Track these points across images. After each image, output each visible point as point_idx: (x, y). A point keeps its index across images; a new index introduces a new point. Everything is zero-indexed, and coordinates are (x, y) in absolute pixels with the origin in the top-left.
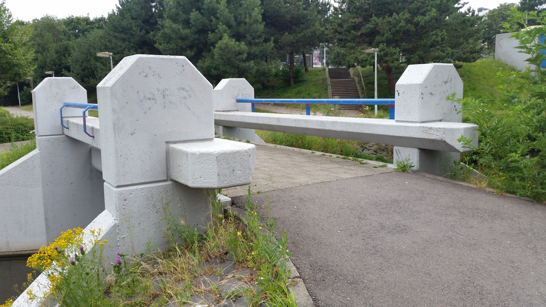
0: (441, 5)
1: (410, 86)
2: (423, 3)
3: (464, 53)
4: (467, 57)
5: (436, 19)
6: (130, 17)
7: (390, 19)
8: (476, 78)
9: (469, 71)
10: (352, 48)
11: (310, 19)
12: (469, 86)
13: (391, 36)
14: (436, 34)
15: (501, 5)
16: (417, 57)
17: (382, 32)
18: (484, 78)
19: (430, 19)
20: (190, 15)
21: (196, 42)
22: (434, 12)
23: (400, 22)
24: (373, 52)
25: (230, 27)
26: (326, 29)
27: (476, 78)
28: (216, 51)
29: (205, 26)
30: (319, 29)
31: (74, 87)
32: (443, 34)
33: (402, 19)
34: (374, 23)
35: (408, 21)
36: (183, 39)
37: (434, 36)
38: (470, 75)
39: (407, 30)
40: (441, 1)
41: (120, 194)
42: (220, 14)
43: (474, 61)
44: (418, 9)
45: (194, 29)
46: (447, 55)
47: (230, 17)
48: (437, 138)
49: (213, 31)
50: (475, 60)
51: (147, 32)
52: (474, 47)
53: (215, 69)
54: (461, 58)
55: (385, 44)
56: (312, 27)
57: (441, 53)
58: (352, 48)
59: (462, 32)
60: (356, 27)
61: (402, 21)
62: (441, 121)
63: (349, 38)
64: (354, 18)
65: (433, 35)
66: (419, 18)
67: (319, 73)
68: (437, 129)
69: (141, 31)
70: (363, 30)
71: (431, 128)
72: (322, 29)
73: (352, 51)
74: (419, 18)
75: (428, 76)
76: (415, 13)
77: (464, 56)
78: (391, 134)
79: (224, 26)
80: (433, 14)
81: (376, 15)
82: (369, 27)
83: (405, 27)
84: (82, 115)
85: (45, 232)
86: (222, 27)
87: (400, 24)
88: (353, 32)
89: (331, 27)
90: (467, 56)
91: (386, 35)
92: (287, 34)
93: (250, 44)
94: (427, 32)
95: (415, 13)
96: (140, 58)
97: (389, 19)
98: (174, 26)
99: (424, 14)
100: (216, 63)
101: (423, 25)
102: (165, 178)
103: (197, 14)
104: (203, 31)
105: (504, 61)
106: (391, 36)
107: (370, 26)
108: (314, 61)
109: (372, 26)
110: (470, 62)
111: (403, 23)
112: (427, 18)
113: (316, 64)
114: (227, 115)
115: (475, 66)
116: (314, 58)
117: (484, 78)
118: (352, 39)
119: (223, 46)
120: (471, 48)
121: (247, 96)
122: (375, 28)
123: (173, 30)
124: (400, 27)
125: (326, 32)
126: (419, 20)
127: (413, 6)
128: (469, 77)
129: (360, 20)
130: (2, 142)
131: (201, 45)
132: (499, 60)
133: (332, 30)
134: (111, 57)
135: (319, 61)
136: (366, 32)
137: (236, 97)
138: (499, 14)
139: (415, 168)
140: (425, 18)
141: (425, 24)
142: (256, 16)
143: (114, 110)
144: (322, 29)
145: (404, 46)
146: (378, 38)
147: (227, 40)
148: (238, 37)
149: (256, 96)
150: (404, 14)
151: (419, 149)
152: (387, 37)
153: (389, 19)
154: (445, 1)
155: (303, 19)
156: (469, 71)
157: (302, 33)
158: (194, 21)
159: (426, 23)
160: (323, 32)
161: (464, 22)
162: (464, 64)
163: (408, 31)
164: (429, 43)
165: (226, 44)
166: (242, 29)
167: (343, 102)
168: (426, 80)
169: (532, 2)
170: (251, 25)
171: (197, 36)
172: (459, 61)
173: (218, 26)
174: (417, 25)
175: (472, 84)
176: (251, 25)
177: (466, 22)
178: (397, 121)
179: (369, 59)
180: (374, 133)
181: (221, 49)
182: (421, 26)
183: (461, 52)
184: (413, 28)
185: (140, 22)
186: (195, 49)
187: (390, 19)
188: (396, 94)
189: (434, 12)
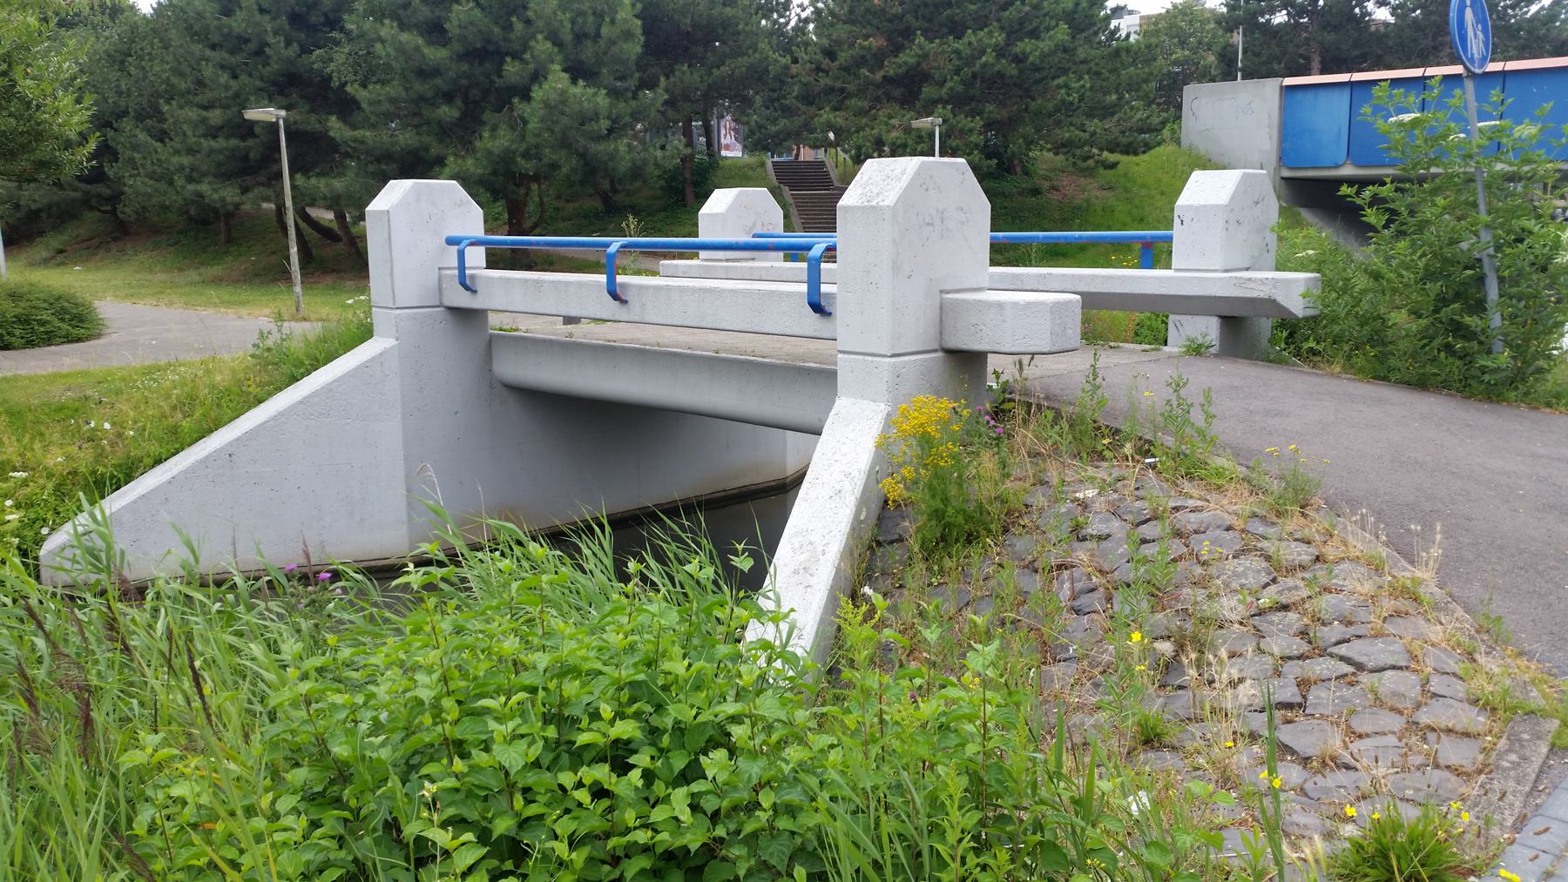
0: (1074, 12)
1: (870, 211)
2: (1036, 7)
3: (1123, 132)
4: (1131, 143)
5: (1065, 50)
6: (256, 7)
7: (957, 45)
8: (1144, 192)
9: (1126, 175)
10: (861, 113)
11: (744, 30)
12: (1129, 212)
13: (960, 88)
14: (1066, 86)
15: (1175, 7)
16: (1021, 140)
17: (937, 75)
18: (1162, 193)
19: (1053, 47)
20: (451, 11)
21: (464, 82)
22: (1062, 33)
23: (983, 52)
24: (929, 126)
25: (558, 43)
26: (795, 61)
27: (1144, 192)
28: (532, 112)
29: (489, 41)
30: (776, 61)
31: (461, 204)
32: (1083, 86)
33: (990, 46)
34: (919, 52)
35: (1001, 52)
36: (424, 73)
37: (1063, 91)
38: (1129, 185)
39: (999, 72)
40: (1077, 5)
41: (895, 366)
42: (535, 11)
43: (1144, 152)
44: (1022, 22)
45: (457, 47)
46: (1092, 136)
47: (561, 21)
48: (1262, 295)
49: (516, 56)
50: (1148, 147)
51: (305, 50)
52: (1148, 117)
53: (526, 155)
54: (1118, 145)
55: (949, 107)
56: (750, 52)
57: (1077, 132)
58: (861, 113)
59: (1113, 78)
60: (878, 59)
61: (989, 50)
62: (1247, 269)
63: (851, 87)
64: (866, 37)
65: (1059, 87)
66: (1024, 46)
67: (750, 173)
68: (1261, 280)
69: (288, 44)
70: (891, 68)
71: (1250, 279)
72: (783, 61)
73: (864, 121)
74: (1024, 46)
75: (1235, 191)
76: (1016, 31)
77: (1124, 140)
78: (1171, 292)
79: (549, 45)
80: (1060, 36)
81: (925, 33)
82: (905, 63)
83: (993, 65)
84: (456, 265)
85: (405, 518)
86: (542, 46)
87: (984, 59)
88: (864, 71)
89: (806, 57)
90: (1131, 139)
91: (949, 84)
92: (685, 67)
93: (614, 93)
94: (1043, 79)
95: (1016, 31)
96: (923, 163)
97: (956, 45)
98: (405, 37)
99: (1035, 34)
100: (531, 140)
101: (1038, 62)
102: (937, 347)
103: (472, 9)
104: (486, 53)
105: (1202, 152)
106: (960, 88)
107: (907, 57)
108: (723, 141)
109: (912, 61)
110: (1136, 153)
111: (988, 58)
112: (1045, 45)
113: (727, 147)
114: (751, 268)
115: (1137, 164)
116: (723, 132)
117: (1162, 193)
118: (859, 90)
119: (553, 97)
120: (1141, 120)
121: (770, 227)
122: (919, 64)
123: (401, 50)
124: (984, 65)
125: (794, 69)
126: (1028, 49)
127: (1011, 14)
128: (1126, 190)
129: (882, 42)
130: (7, 347)
131: (475, 93)
132: (1190, 148)
133: (809, 65)
134: (281, 122)
135: (736, 139)
136: (897, 75)
137: (751, 229)
138: (1171, 28)
139: (1212, 350)
140: (1041, 45)
141: (1042, 62)
142: (626, 21)
143: (894, 241)
144: (783, 61)
145: (990, 112)
146: (928, 91)
147: (558, 80)
148: (577, 71)
149: (487, 231)
150: (990, 33)
151: (1220, 317)
152: (951, 89)
153: (956, 45)
154: (1084, 5)
155: (724, 29)
156: (1126, 175)
157: (722, 68)
158: (460, 27)
159: (1044, 56)
160: (787, 68)
161: (1117, 52)
162: (1124, 159)
163: (1000, 75)
164: (1050, 106)
165: (563, 92)
166: (588, 52)
167: (1045, 237)
168: (1233, 198)
169: (1253, 4)
170: (612, 42)
171: (465, 67)
172: (1112, 151)
173: (532, 43)
174: (1019, 60)
175: (1137, 207)
176: (612, 42)
177: (1124, 55)
178: (1177, 270)
179: (910, 142)
180: (1137, 291)
181: (547, 104)
182: (1032, 64)
183: (1116, 131)
184: (1012, 70)
185: (283, 21)
186: (459, 102)
187: (957, 45)
188: (1177, 221)
189: (1062, 33)
